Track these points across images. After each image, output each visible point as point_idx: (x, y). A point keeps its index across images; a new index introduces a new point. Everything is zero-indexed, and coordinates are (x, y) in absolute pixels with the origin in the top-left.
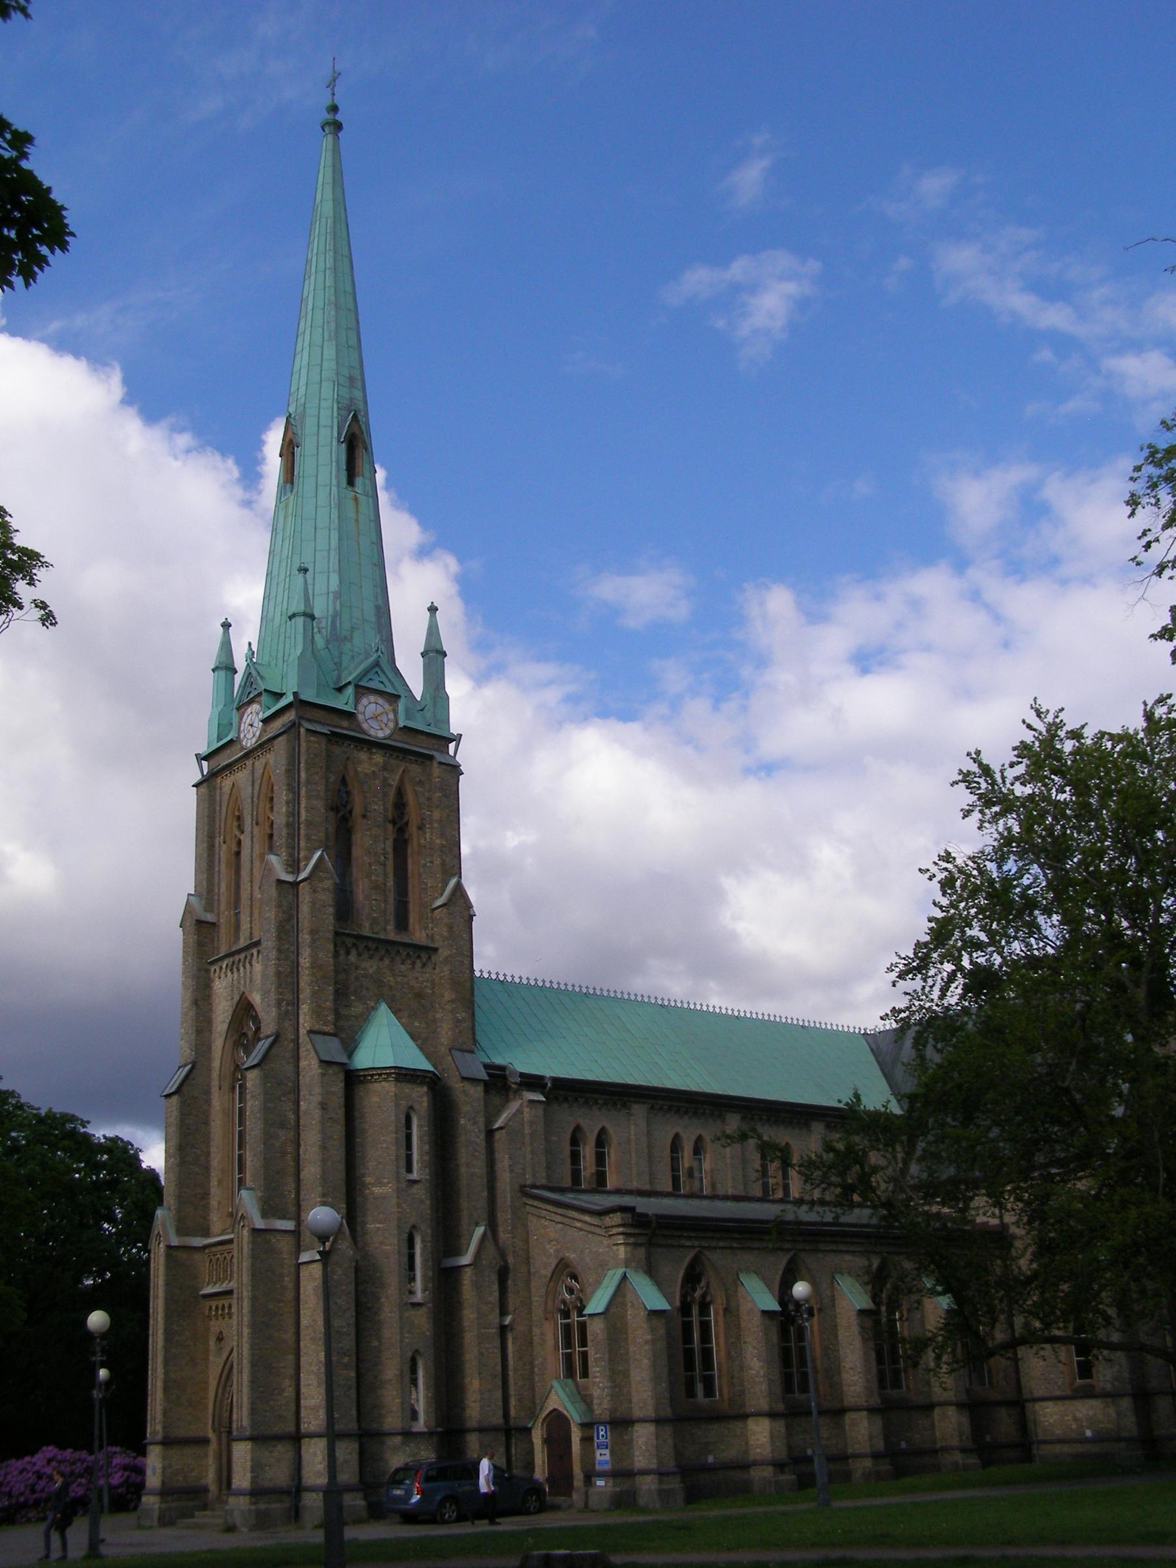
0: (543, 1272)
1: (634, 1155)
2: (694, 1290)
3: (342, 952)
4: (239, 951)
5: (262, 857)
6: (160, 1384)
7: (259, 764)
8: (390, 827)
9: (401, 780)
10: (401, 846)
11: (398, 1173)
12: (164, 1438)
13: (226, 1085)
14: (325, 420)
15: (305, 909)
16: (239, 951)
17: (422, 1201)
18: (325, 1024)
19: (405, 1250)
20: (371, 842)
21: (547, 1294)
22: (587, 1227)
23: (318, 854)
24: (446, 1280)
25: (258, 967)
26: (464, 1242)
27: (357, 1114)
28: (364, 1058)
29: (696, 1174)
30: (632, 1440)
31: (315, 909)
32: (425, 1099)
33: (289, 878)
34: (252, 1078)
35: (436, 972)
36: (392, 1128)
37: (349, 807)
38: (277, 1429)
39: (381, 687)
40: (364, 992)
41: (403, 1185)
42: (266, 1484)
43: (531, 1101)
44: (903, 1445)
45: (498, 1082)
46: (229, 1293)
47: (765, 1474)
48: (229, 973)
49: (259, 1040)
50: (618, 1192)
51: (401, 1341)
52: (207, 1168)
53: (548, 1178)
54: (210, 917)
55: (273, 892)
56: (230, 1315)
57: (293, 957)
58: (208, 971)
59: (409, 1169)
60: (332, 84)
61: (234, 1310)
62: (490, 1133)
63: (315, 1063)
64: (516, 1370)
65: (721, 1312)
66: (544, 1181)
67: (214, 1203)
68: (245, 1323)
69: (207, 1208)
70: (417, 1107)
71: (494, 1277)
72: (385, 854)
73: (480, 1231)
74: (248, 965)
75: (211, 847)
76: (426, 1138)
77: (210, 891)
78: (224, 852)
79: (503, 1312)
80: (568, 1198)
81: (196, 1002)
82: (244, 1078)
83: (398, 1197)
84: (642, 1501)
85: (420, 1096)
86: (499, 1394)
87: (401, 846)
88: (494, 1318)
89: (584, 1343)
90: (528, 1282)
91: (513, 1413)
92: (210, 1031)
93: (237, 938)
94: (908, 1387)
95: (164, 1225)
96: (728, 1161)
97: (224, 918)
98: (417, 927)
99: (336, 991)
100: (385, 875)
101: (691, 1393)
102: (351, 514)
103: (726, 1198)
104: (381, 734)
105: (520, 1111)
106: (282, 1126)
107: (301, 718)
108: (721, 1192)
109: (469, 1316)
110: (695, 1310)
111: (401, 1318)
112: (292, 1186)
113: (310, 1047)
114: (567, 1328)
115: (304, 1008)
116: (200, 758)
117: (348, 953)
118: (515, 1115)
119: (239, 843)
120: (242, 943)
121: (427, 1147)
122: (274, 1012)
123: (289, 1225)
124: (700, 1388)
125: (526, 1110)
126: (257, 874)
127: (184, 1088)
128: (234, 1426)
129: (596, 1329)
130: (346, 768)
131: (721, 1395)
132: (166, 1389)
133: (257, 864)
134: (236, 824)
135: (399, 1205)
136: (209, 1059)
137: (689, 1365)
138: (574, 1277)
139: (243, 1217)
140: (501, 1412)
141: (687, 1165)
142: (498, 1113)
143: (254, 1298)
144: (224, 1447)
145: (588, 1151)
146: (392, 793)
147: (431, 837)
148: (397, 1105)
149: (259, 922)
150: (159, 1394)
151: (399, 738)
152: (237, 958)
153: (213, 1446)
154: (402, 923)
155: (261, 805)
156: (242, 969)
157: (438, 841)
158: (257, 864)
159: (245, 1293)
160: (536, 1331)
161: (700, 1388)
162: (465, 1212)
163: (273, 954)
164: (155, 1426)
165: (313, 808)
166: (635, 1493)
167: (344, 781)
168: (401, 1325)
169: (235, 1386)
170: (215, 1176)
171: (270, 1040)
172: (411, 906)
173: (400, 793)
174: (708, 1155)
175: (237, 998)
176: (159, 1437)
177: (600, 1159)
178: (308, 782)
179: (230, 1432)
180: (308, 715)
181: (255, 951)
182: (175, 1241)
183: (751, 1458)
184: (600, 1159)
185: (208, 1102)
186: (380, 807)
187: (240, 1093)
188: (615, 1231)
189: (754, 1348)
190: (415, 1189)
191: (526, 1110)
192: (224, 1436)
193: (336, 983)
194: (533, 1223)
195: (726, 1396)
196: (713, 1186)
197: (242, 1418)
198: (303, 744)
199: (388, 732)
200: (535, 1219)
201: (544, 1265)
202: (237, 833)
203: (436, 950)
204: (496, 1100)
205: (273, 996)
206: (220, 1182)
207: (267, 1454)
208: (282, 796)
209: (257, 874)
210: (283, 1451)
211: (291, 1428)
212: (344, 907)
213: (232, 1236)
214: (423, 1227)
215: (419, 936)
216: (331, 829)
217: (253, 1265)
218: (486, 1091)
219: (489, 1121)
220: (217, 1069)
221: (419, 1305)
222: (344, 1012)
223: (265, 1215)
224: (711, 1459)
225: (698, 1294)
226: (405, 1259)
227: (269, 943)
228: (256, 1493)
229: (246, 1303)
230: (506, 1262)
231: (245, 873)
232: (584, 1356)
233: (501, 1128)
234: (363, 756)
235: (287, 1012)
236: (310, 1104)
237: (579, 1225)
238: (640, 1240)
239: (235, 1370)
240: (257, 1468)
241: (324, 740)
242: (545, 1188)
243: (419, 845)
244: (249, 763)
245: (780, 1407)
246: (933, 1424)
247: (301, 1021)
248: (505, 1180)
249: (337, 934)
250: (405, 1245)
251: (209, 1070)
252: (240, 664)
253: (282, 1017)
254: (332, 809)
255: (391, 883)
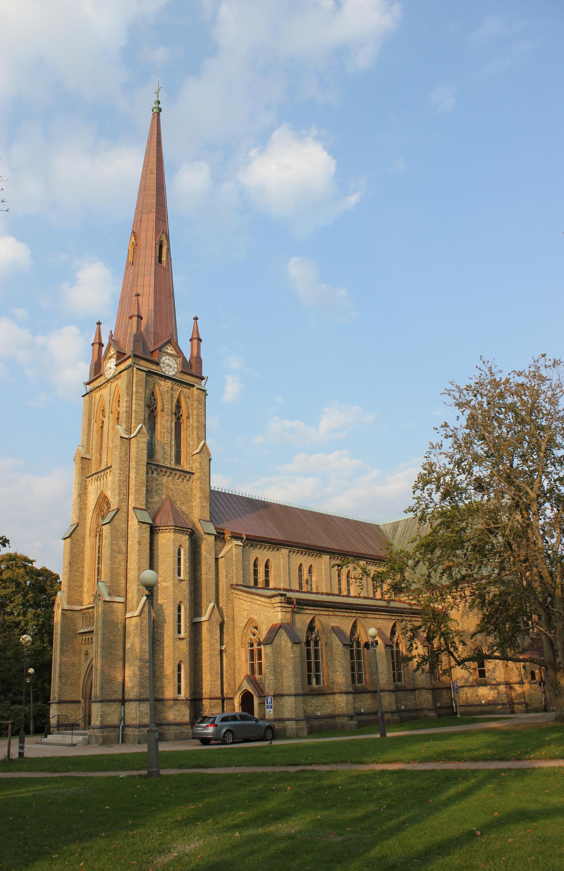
0: (241, 625)
1: (282, 573)
2: (312, 634)
3: (150, 472)
4: (101, 472)
5: (113, 428)
6: (57, 675)
7: (113, 385)
9: (179, 395)
11: (174, 576)
12: (59, 700)
13: (93, 535)
15: (133, 451)
16: (101, 472)
17: (185, 590)
18: (141, 505)
19: (177, 613)
20: (164, 422)
21: (242, 636)
22: (262, 603)
23: (140, 425)
24: (195, 627)
25: (110, 478)
26: (203, 610)
27: (155, 548)
29: (310, 583)
30: (283, 705)
31: (139, 448)
32: (187, 542)
33: (127, 436)
34: (106, 529)
35: (194, 484)
36: (172, 555)
37: (155, 406)
38: (114, 697)
40: (160, 491)
41: (176, 582)
42: (108, 723)
43: (236, 545)
44: (403, 707)
46: (92, 632)
47: (344, 721)
48: (96, 482)
49: (110, 512)
50: (275, 589)
51: (174, 657)
52: (83, 573)
53: (244, 581)
54: (88, 456)
55: (118, 442)
56: (92, 643)
57: (127, 473)
58: (86, 481)
59: (179, 575)
60: (157, 93)
61: (94, 639)
62: (217, 559)
63: (136, 522)
64: (227, 671)
65: (324, 645)
66: (242, 583)
67: (85, 590)
68: (99, 646)
69: (82, 592)
70: (183, 545)
71: (218, 627)
72: (171, 428)
73: (212, 605)
74: (105, 478)
75: (89, 424)
76: (188, 560)
77: (88, 444)
78: (95, 427)
79: (222, 644)
80: (253, 590)
81: (80, 496)
82: (101, 530)
83: (174, 588)
84: (288, 733)
88: (218, 646)
89: (260, 658)
90: (233, 630)
91: (225, 691)
92: (86, 509)
93: (100, 466)
94: (405, 681)
95: (61, 599)
96: (324, 577)
97: (94, 457)
98: (185, 463)
99: (147, 490)
100: (171, 438)
101: (310, 683)
103: (322, 594)
104: (171, 374)
105: (231, 549)
106: (119, 552)
107: (134, 363)
108: (320, 591)
109: (205, 645)
110: (312, 643)
111: (174, 645)
112: (123, 581)
113: (134, 515)
114: (252, 652)
115: (131, 497)
117: (153, 473)
118: (228, 551)
119: (103, 422)
120: (103, 468)
121: (188, 565)
122: (117, 498)
123: (122, 600)
124: (314, 680)
125: (234, 549)
126: (111, 436)
127: (72, 535)
128: (93, 695)
130: (154, 387)
131: (323, 684)
132: (60, 677)
133: (111, 431)
134: (101, 413)
135: (174, 591)
136: (85, 522)
137: (309, 670)
138: (256, 628)
139: (99, 595)
140: (220, 691)
141: (305, 578)
142: (221, 551)
143: (104, 634)
144: (87, 705)
145: (261, 570)
147: (193, 422)
148: (174, 545)
149: (112, 456)
150: (57, 679)
151: (179, 376)
152: (100, 474)
153: (83, 704)
154: (178, 460)
155: (114, 404)
156: (102, 480)
157: (196, 424)
158: (111, 431)
159: (99, 632)
160: (237, 653)
161: (314, 680)
162: (205, 596)
163: (118, 471)
164: (54, 694)
165: (139, 406)
166: (285, 729)
167: (153, 394)
168: (174, 649)
169: (93, 676)
170: (86, 577)
171: (115, 512)
172: (182, 453)
173: (178, 401)
174: (315, 574)
175: (99, 493)
176: (56, 701)
177: (267, 573)
178: (137, 392)
179: (90, 698)
180: (137, 362)
181: (108, 471)
182: (66, 607)
183: (336, 713)
184: (267, 573)
185: (84, 542)
186: (169, 407)
187: (99, 539)
188: (277, 605)
189: (339, 662)
191: (234, 549)
192: (87, 700)
193: (147, 486)
194: (236, 602)
195: (326, 685)
196: (317, 588)
197: (96, 691)
198: (135, 375)
199: (174, 373)
200: (237, 600)
201: (241, 621)
202: (102, 418)
203: (193, 474)
204: (220, 545)
205: (117, 491)
206: (88, 580)
207: (108, 709)
208: (124, 399)
209: (111, 436)
210: (116, 707)
211: (120, 697)
212: (151, 452)
213: (94, 605)
214: (185, 602)
215: (185, 466)
216: (147, 416)
217: (103, 618)
218: (215, 540)
219: (216, 554)
220: (89, 527)
221: (183, 639)
222: (150, 500)
223: (110, 595)
224: (319, 714)
225: (313, 636)
226: (177, 617)
227: (116, 467)
228: (103, 727)
229: (100, 637)
230: (223, 620)
231: (105, 436)
232: (260, 664)
233: (221, 557)
234: (162, 383)
235: (123, 499)
236: (133, 543)
237: (259, 602)
238: (289, 610)
239: (94, 668)
240: (103, 715)
241: (144, 374)
242: (242, 586)
243: (187, 426)
244: (109, 385)
245: (351, 689)
246: (415, 698)
247: (130, 503)
249: (148, 463)
250: (177, 610)
251: (85, 527)
253: (121, 501)
254: (147, 406)
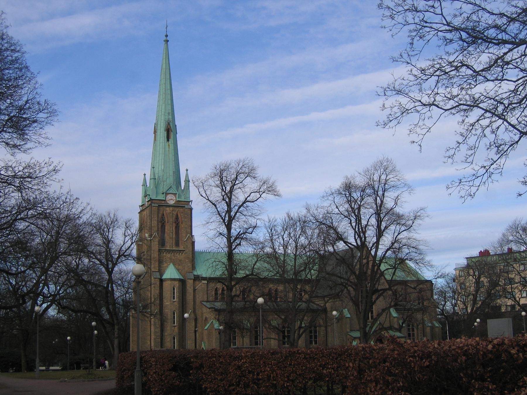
8: (174, 224)
10: (177, 228)
14: (162, 126)
28: (166, 276)
39: (172, 192)
45: (197, 278)
59: (174, 299)
85: (177, 284)
86: (194, 344)
87: (177, 228)
102: (167, 149)
116: (140, 206)
129: (206, 332)
146: (174, 216)
190: (175, 303)
212: (162, 243)
248: (198, 300)
252: (156, 177)
255: (174, 236)
